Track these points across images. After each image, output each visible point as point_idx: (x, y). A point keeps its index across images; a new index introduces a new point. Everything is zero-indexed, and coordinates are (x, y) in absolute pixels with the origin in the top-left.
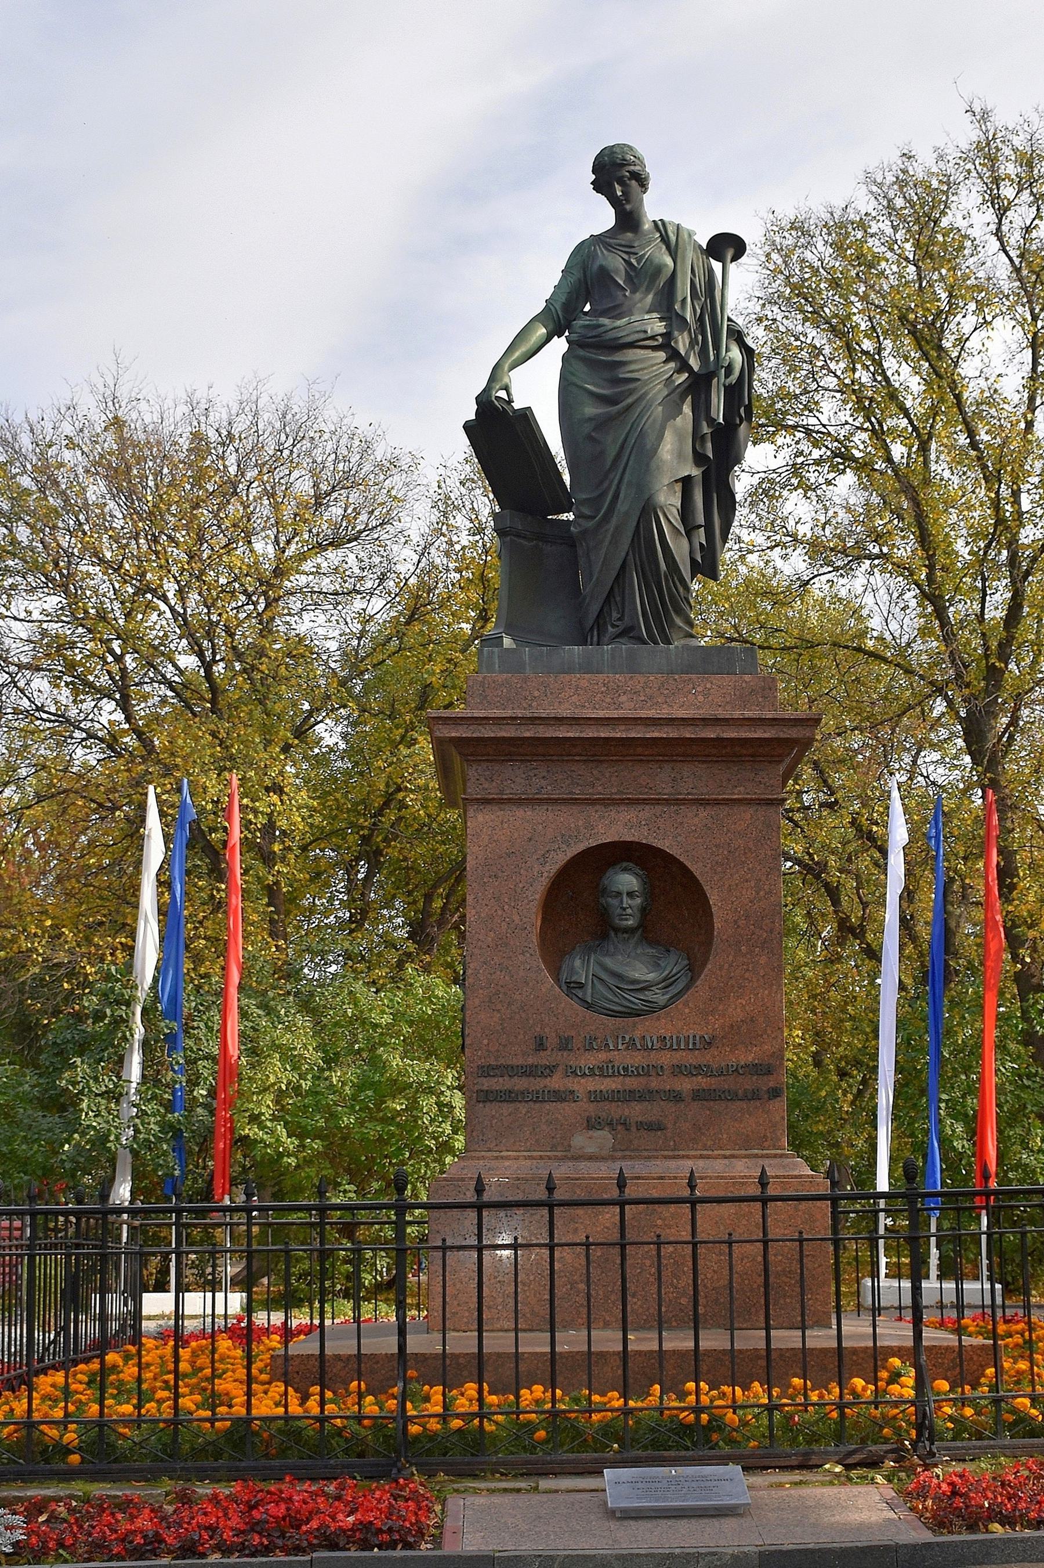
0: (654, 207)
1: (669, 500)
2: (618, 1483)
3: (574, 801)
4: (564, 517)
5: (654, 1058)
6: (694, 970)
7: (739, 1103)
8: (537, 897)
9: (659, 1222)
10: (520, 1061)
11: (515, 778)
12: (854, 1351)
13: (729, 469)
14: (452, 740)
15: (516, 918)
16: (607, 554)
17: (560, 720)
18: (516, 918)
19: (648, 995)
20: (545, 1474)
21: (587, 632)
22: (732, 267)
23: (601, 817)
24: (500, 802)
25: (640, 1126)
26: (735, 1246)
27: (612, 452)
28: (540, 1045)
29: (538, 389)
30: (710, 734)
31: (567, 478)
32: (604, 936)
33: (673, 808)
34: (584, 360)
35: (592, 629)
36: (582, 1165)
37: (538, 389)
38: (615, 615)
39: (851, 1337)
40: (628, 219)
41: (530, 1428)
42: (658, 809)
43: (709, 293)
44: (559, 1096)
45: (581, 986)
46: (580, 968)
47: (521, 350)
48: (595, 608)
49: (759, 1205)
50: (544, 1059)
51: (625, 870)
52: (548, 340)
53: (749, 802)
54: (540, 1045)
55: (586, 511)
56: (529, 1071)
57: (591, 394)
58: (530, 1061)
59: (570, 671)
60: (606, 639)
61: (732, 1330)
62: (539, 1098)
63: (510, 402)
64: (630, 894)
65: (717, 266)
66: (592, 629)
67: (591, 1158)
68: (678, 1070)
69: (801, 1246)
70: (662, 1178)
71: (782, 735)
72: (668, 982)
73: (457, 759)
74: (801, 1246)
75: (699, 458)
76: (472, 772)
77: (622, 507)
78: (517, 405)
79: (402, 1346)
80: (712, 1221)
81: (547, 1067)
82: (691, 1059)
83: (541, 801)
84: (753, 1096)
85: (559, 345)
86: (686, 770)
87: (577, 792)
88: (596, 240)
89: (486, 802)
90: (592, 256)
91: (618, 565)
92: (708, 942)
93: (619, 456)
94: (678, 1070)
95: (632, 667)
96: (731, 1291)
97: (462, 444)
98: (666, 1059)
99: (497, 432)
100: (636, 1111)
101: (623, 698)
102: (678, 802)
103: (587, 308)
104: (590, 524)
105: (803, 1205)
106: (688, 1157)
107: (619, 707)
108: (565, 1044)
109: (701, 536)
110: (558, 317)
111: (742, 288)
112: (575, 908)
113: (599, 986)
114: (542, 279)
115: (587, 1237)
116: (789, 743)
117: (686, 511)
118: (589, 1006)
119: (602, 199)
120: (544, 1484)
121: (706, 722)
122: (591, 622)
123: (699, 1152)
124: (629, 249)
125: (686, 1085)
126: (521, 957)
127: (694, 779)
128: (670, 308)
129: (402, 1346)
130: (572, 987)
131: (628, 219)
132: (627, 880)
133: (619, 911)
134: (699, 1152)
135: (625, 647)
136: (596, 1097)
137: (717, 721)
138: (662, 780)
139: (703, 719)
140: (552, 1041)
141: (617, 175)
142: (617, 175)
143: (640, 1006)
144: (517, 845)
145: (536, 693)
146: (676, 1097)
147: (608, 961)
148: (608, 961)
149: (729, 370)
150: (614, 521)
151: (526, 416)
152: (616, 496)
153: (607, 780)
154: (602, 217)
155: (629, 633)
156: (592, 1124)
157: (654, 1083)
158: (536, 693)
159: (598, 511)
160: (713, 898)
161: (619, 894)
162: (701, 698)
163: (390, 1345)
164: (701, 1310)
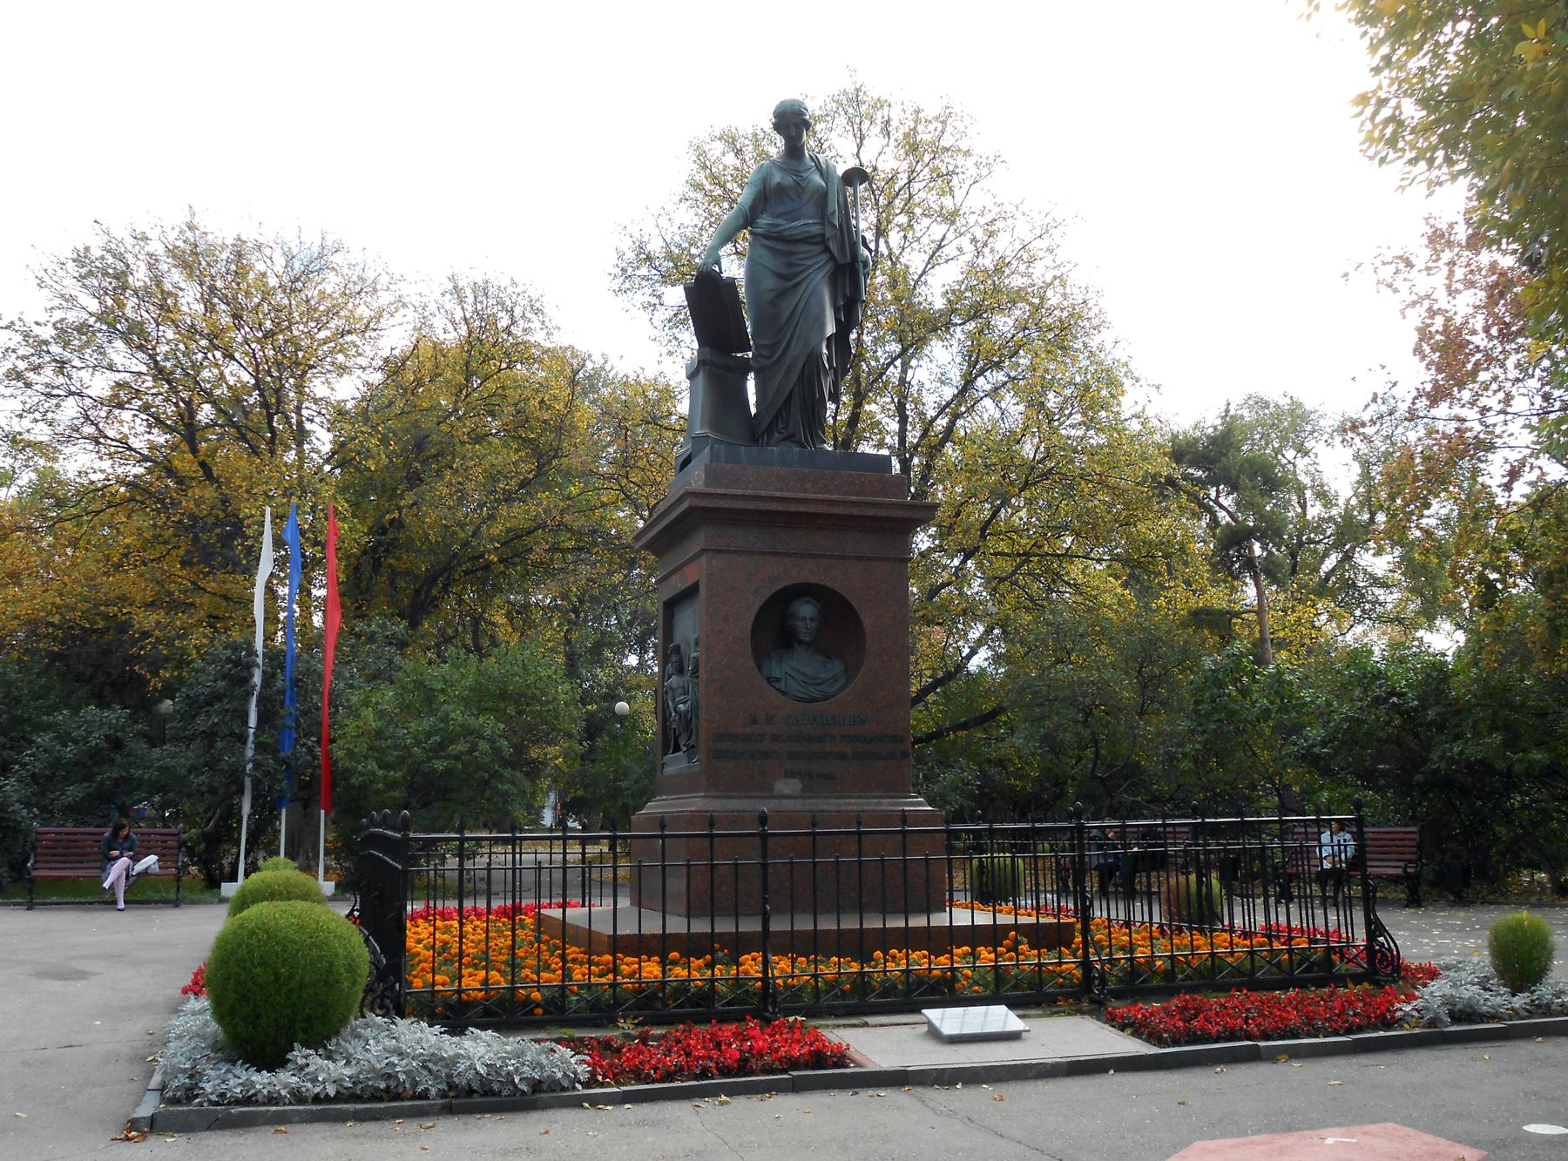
2: (949, 1019)
3: (775, 554)
12: (804, 911)
24: (728, 552)
27: (786, 314)
28: (755, 721)
34: (768, 248)
36: (784, 801)
38: (781, 425)
40: (794, 150)
45: (778, 680)
57: (774, 273)
58: (748, 730)
60: (773, 440)
67: (787, 797)
72: (835, 679)
78: (724, 275)
93: (790, 317)
102: (844, 557)
113: (790, 681)
118: (783, 693)
124: (797, 173)
143: (816, 694)
146: (842, 757)
152: (788, 345)
154: (776, 147)
156: (788, 774)
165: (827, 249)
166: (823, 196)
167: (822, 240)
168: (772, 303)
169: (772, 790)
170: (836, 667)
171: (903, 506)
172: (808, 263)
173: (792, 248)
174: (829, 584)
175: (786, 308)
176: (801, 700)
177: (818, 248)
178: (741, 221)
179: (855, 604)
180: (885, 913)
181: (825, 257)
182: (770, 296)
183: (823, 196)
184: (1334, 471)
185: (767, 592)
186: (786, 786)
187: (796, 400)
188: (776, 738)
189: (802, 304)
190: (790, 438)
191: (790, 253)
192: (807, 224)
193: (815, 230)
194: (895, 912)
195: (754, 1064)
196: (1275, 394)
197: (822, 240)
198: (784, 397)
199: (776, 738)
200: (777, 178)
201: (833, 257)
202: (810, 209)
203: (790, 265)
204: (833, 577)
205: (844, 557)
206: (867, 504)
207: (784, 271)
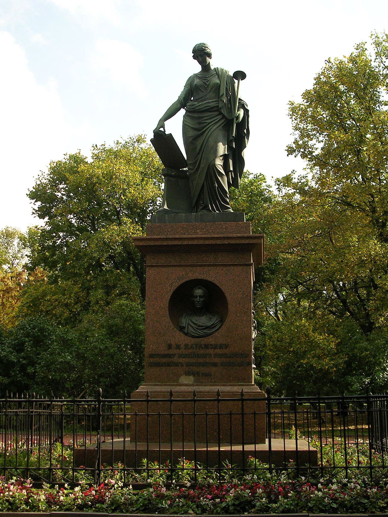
0: (214, 63)
1: (219, 162)
4: (185, 169)
6: (222, 321)
7: (236, 367)
8: (169, 298)
9: (207, 407)
10: (163, 353)
15: (162, 305)
16: (199, 180)
18: (162, 305)
22: (241, 81)
23: (191, 271)
24: (157, 266)
26: (232, 415)
27: (199, 148)
29: (175, 128)
30: (226, 242)
33: (215, 267)
35: (194, 207)
37: (175, 128)
38: (201, 202)
39: (287, 448)
42: (210, 268)
44: (176, 365)
46: (184, 321)
47: (170, 114)
49: (241, 402)
50: (172, 352)
51: (199, 288)
53: (241, 265)
54: (170, 346)
55: (191, 167)
56: (165, 356)
57: (192, 128)
58: (166, 353)
62: (168, 365)
63: (165, 131)
65: (236, 81)
66: (194, 207)
67: (186, 385)
68: (216, 355)
69: (255, 416)
70: (209, 392)
71: (251, 242)
74: (255, 416)
77: (202, 166)
81: (171, 355)
85: (183, 112)
88: (196, 76)
90: (193, 81)
91: (201, 185)
96: (231, 431)
98: (211, 351)
101: (198, 231)
103: (192, 99)
104: (192, 172)
105: (256, 402)
106: (218, 385)
107: (197, 234)
110: (182, 103)
115: (231, 412)
116: (253, 245)
117: (226, 166)
118: (186, 334)
119: (196, 61)
122: (193, 205)
123: (222, 384)
126: (163, 318)
130: (182, 329)
131: (206, 67)
132: (199, 292)
133: (197, 302)
134: (222, 384)
136: (188, 365)
139: (224, 237)
140: (182, 346)
141: (201, 54)
142: (201, 54)
145: (169, 230)
146: (215, 365)
149: (238, 117)
154: (197, 68)
156: (188, 374)
158: (169, 230)
159: (195, 167)
161: (197, 297)
162: (224, 230)
164: (221, 437)
165: (221, 113)
166: (217, 87)
169: (178, 382)
170: (214, 320)
171: (248, 238)
172: (209, 121)
173: (201, 115)
174: (210, 279)
176: (193, 337)
177: (216, 113)
178: (179, 106)
180: (231, 444)
181: (220, 117)
183: (217, 87)
185: (177, 284)
186: (184, 379)
187: (205, 188)
188: (180, 356)
189: (206, 141)
191: (199, 118)
192: (211, 102)
194: (238, 443)
195: (17, 404)
197: (217, 109)
198: (200, 188)
199: (180, 356)
200: (197, 81)
201: (224, 117)
202: (211, 95)
204: (212, 275)
206: (224, 238)
207: (197, 127)
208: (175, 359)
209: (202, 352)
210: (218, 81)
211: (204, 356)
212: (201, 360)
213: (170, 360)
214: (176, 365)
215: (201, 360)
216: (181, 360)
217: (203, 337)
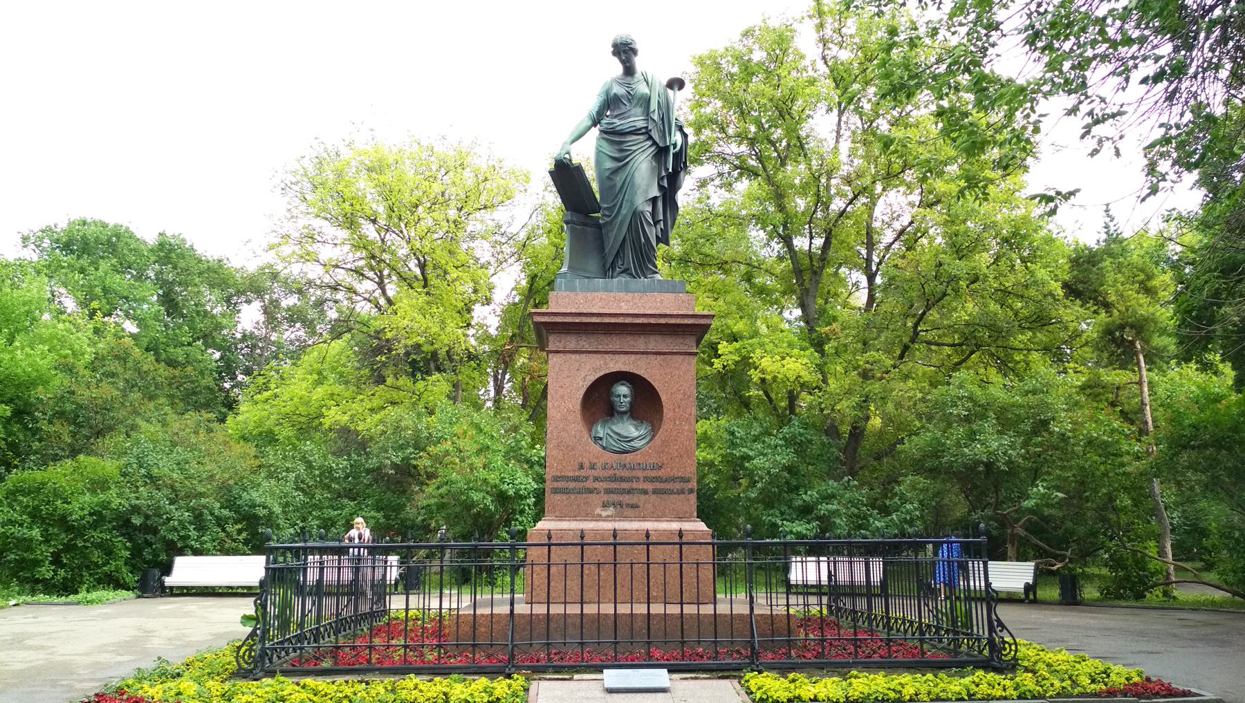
0: (640, 63)
3: (599, 352)
5: (634, 473)
6: (654, 430)
10: (571, 474)
11: (571, 342)
13: (675, 192)
14: (542, 323)
17: (592, 315)
19: (632, 444)
20: (578, 672)
21: (607, 270)
24: (564, 352)
25: (628, 505)
27: (619, 185)
31: (598, 196)
32: (612, 415)
34: (607, 140)
41: (777, 476)
43: (666, 108)
44: (590, 491)
45: (601, 439)
46: (600, 431)
48: (610, 260)
50: (583, 473)
52: (589, 128)
53: (681, 354)
54: (581, 467)
56: (576, 479)
59: (598, 290)
61: (665, 603)
64: (625, 396)
68: (646, 479)
73: (544, 332)
75: (661, 187)
76: (551, 338)
77: (624, 211)
79: (512, 611)
80: (657, 553)
82: (653, 474)
83: (583, 352)
84: (682, 492)
85: (595, 132)
86: (652, 338)
87: (600, 348)
89: (558, 352)
92: (661, 419)
94: (646, 479)
95: (627, 290)
97: (549, 179)
99: (566, 175)
100: (626, 499)
102: (647, 353)
104: (607, 219)
108: (592, 467)
109: (662, 225)
111: (681, 102)
112: (598, 402)
114: (592, 103)
117: (654, 214)
118: (604, 448)
120: (576, 677)
121: (661, 316)
125: (649, 486)
127: (655, 343)
128: (648, 115)
129: (512, 611)
131: (629, 71)
132: (623, 389)
135: (624, 279)
136: (608, 491)
137: (666, 316)
138: (640, 343)
140: (587, 465)
141: (625, 51)
142: (625, 51)
144: (570, 375)
146: (645, 492)
147: (614, 428)
148: (614, 428)
149: (675, 145)
150: (620, 218)
151: (579, 169)
153: (615, 343)
154: (617, 68)
155: (626, 271)
156: (605, 506)
157: (635, 485)
160: (663, 398)
163: (505, 610)
165: (650, 138)
167: (647, 133)
168: (609, 178)
175: (619, 179)
178: (590, 123)
179: (655, 385)
181: (649, 143)
182: (607, 173)
183: (646, 101)
184: (1195, 175)
185: (592, 378)
188: (596, 479)
190: (625, 271)
192: (636, 119)
193: (641, 124)
196: (111, 220)
199: (596, 479)
201: (655, 143)
203: (622, 151)
205: (647, 353)
208: (589, 484)
209: (626, 474)
210: (647, 91)
211: (629, 480)
212: (625, 485)
213: (581, 485)
214: (590, 491)
215: (625, 485)
216: (597, 485)
217: (627, 452)
